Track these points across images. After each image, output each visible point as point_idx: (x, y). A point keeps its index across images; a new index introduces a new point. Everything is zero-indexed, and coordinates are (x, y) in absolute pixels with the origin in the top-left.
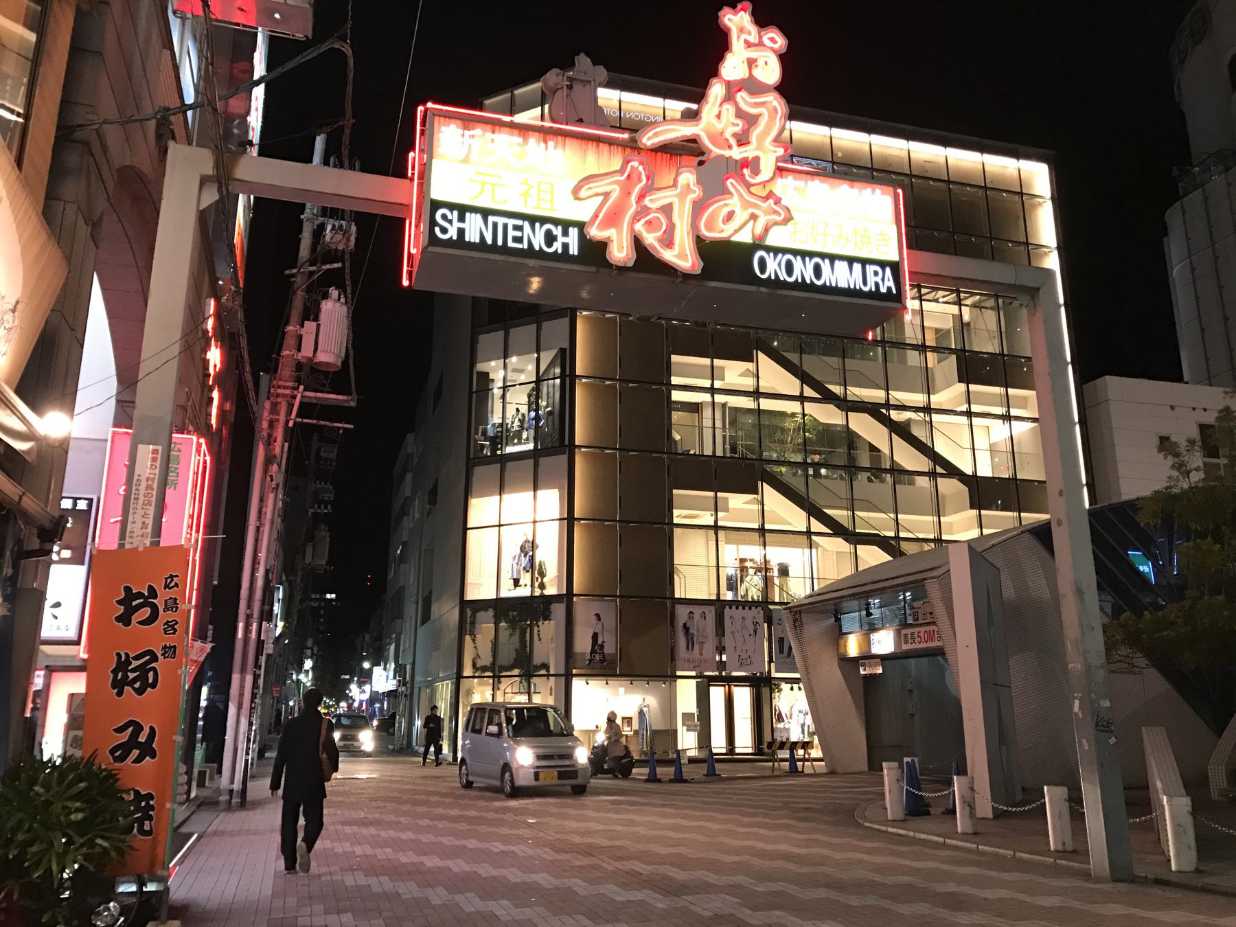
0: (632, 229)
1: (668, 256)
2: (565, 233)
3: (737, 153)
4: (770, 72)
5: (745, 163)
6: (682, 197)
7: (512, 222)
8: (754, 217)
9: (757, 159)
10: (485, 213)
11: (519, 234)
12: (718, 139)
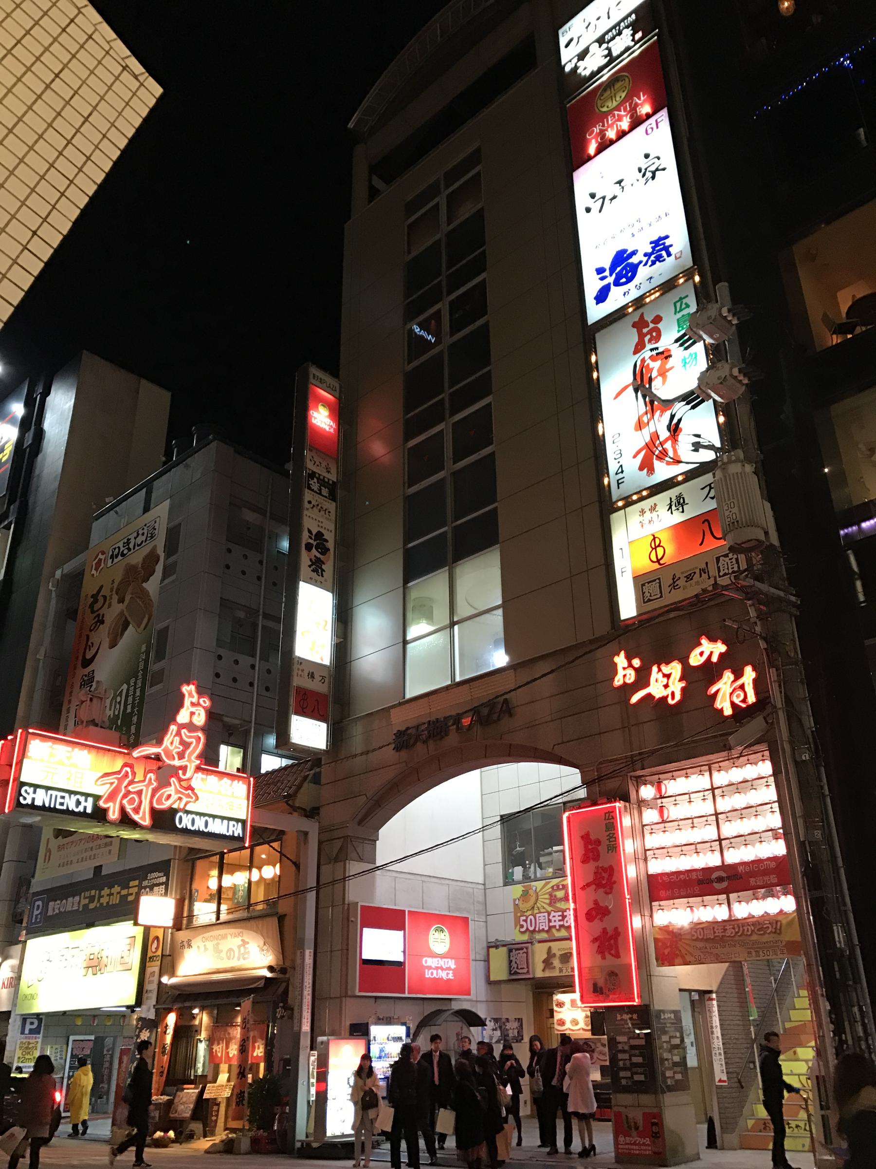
0: (121, 803)
1: (136, 817)
2: (86, 801)
3: (177, 763)
4: (200, 719)
5: (181, 768)
6: (147, 786)
7: (60, 794)
8: (180, 799)
9: (186, 767)
10: (47, 788)
11: (62, 801)
12: (168, 753)
